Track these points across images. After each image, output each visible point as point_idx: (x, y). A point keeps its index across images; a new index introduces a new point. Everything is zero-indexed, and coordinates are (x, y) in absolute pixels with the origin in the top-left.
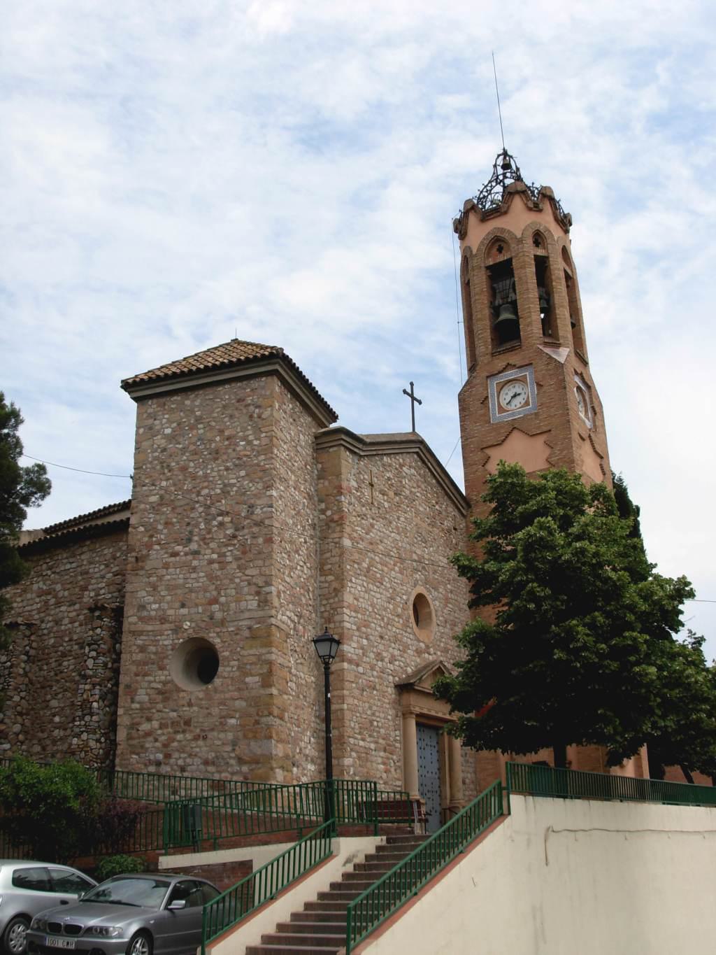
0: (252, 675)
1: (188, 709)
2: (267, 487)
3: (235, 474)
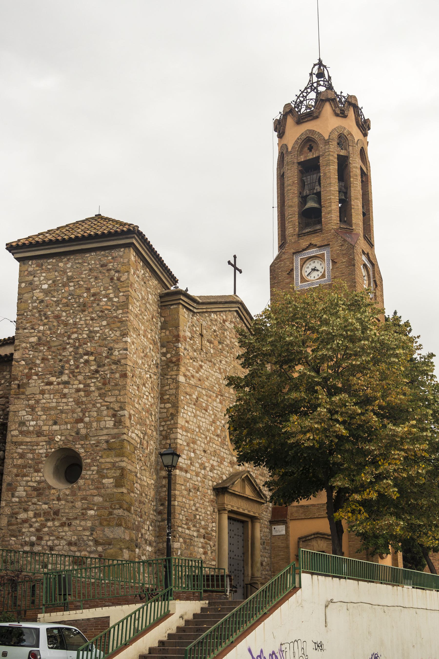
0: (108, 478)
1: (57, 502)
2: (124, 335)
3: (98, 323)
